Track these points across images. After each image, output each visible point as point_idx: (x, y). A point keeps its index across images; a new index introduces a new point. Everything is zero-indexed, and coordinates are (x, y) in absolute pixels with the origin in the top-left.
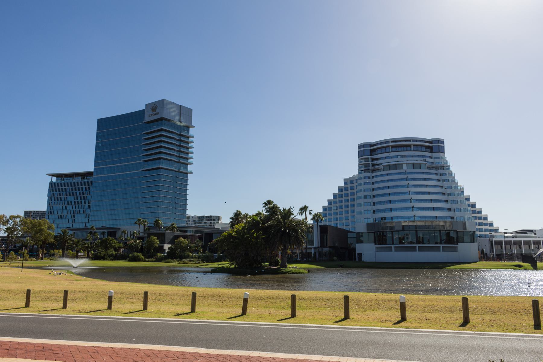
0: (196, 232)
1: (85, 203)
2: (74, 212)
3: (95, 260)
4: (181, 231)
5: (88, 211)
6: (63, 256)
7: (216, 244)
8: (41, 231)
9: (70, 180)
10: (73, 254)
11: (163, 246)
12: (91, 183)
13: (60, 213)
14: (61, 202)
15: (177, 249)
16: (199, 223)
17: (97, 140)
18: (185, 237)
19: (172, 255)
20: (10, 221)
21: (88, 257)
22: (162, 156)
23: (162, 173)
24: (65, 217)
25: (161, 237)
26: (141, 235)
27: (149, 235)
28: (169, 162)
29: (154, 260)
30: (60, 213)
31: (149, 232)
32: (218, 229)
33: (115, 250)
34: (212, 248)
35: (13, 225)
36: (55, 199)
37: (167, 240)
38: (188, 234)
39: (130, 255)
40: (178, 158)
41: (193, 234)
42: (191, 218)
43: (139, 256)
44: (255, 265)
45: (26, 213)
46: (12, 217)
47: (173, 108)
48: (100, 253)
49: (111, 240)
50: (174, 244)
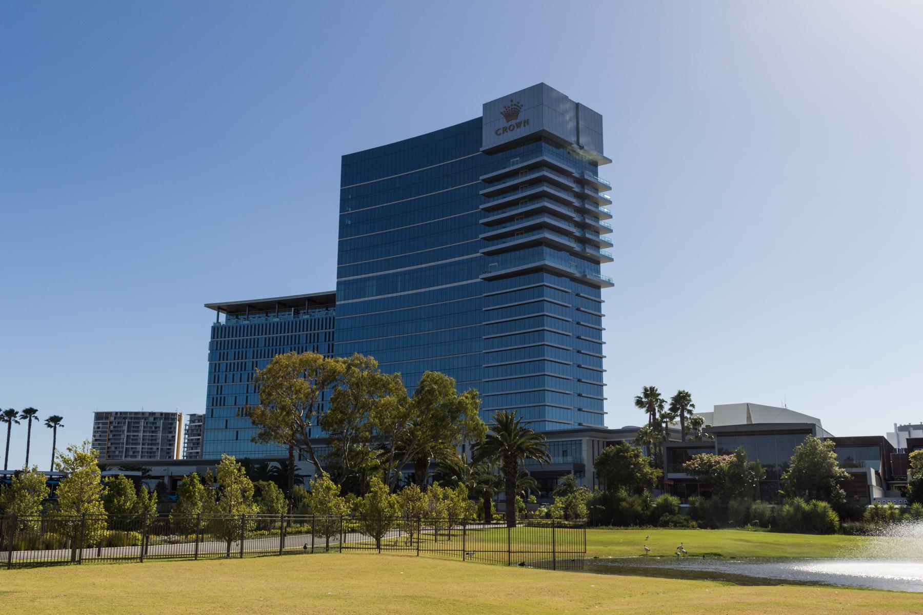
9: (258, 319)
13: (241, 401)
14: (245, 376)
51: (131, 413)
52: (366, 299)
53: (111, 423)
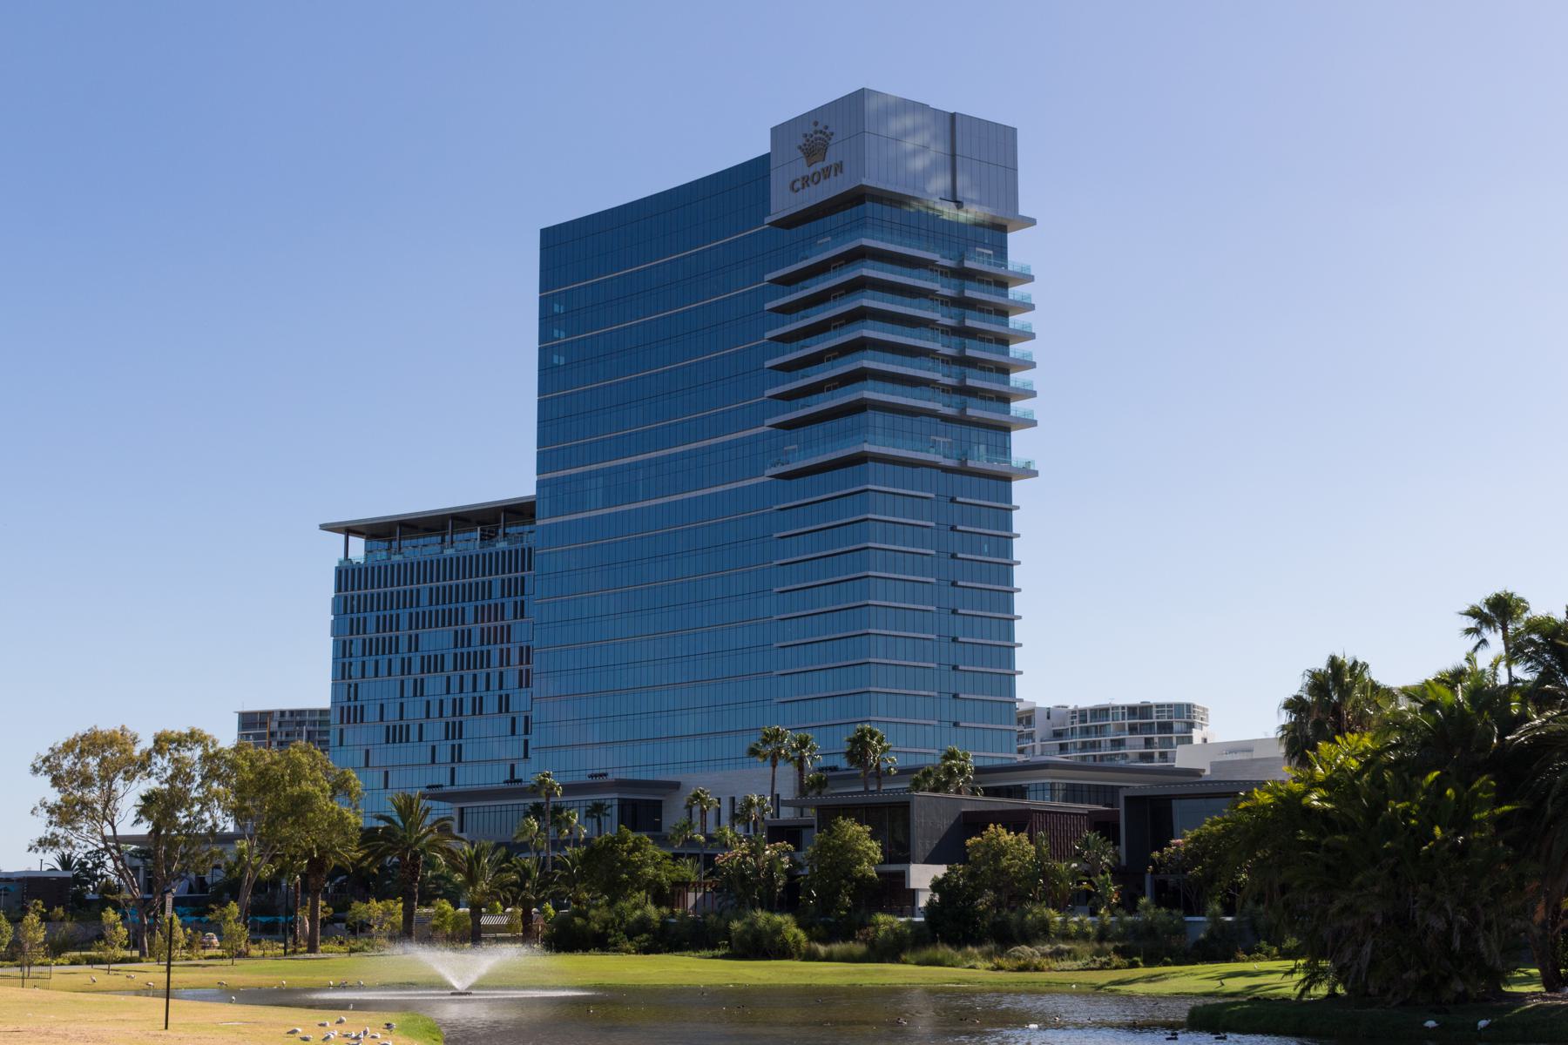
0: (1073, 793)
1: (505, 659)
2: (458, 707)
3: (558, 950)
4: (989, 792)
5: (519, 701)
6: (407, 932)
7: (1193, 856)
8: (303, 803)
10: (458, 920)
11: (902, 877)
12: (524, 559)
13: (392, 715)
15: (978, 891)
16: (1084, 746)
17: (544, 336)
18: (1016, 822)
19: (953, 924)
20: (160, 762)
21: (527, 935)
22: (867, 364)
23: (876, 480)
24: (414, 735)
25: (891, 821)
26: (787, 814)
27: (828, 814)
28: (907, 420)
29: (859, 948)
30: (392, 715)
31: (826, 801)
32: (1196, 773)
33: (659, 898)
34: (1171, 880)
35: (173, 777)
36: (369, 648)
37: (921, 844)
38: (1032, 802)
39: (736, 925)
40: (957, 399)
41: (1059, 805)
42: (1039, 719)
43: (777, 930)
44: (1458, 986)
45: (249, 722)
46: (163, 743)
47: (914, 131)
48: (584, 915)
49: (636, 848)
50: (964, 860)
51: (312, 712)
52: (586, 514)
53: (272, 734)
